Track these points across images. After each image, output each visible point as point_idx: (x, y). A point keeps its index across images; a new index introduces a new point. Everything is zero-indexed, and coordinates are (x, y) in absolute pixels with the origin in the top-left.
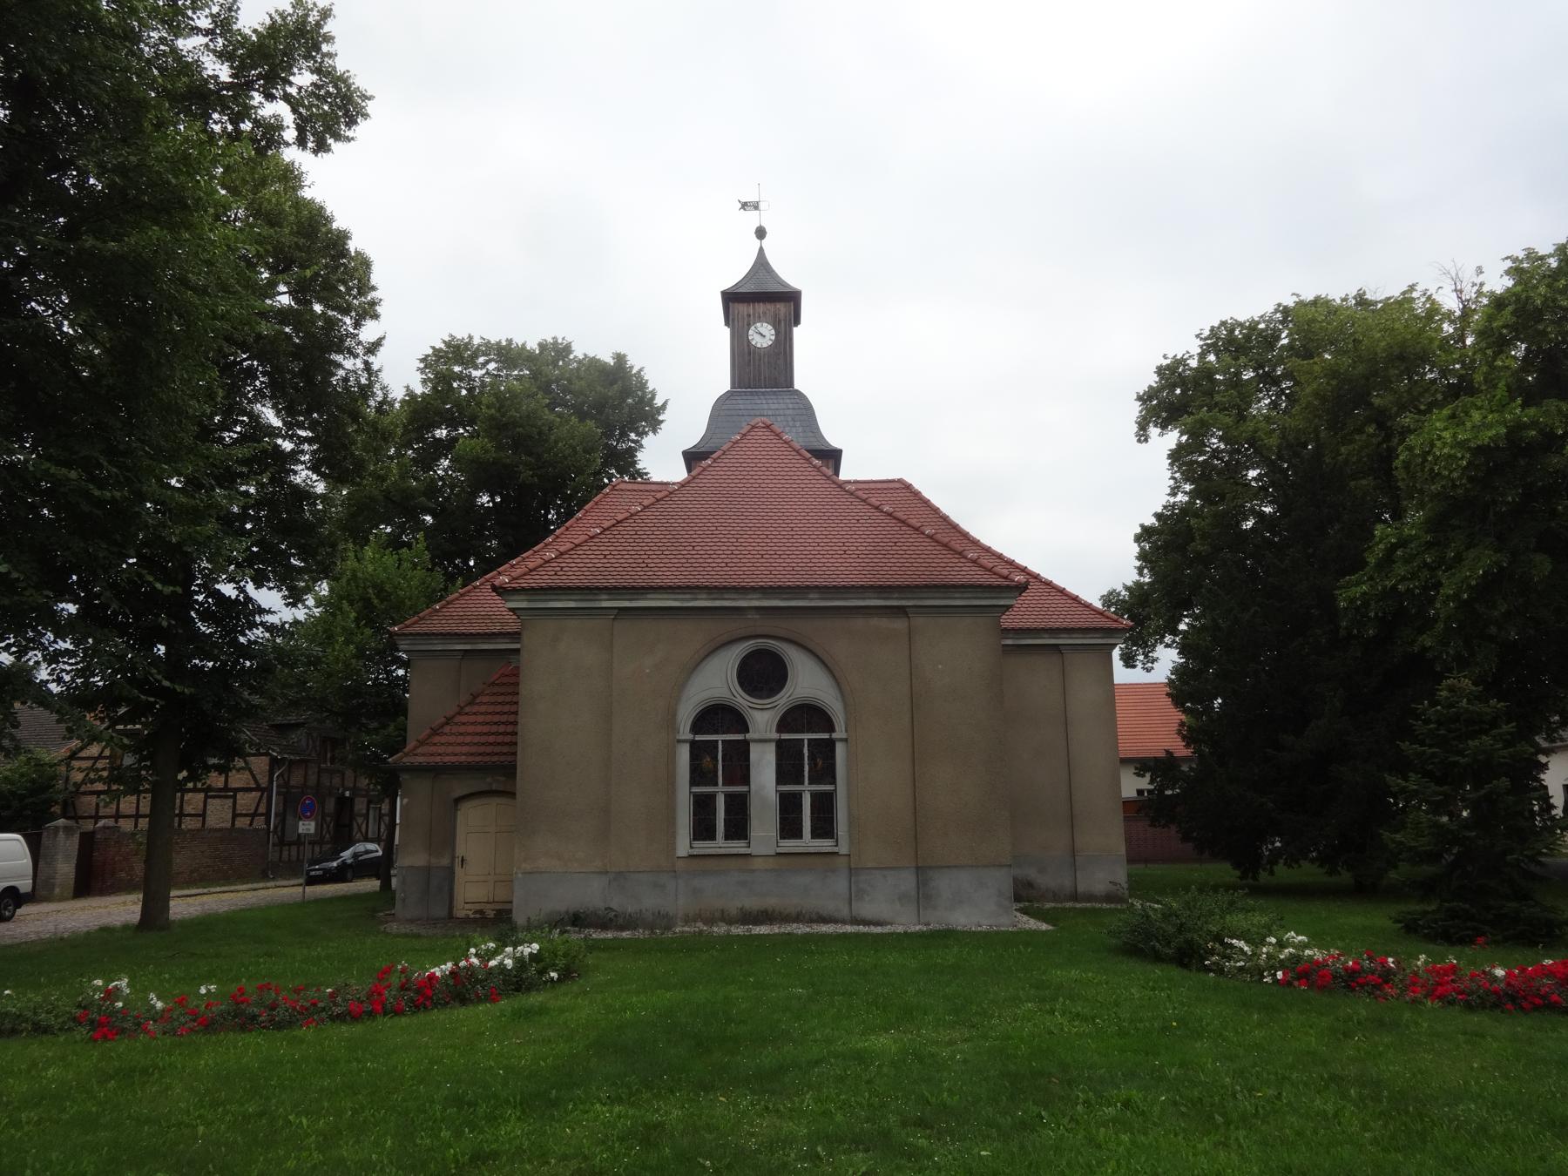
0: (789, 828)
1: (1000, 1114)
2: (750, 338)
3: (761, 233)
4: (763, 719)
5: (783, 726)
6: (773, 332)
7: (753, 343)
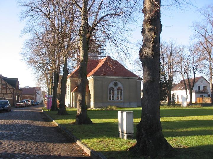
0: (118, 99)
4: (116, 88)
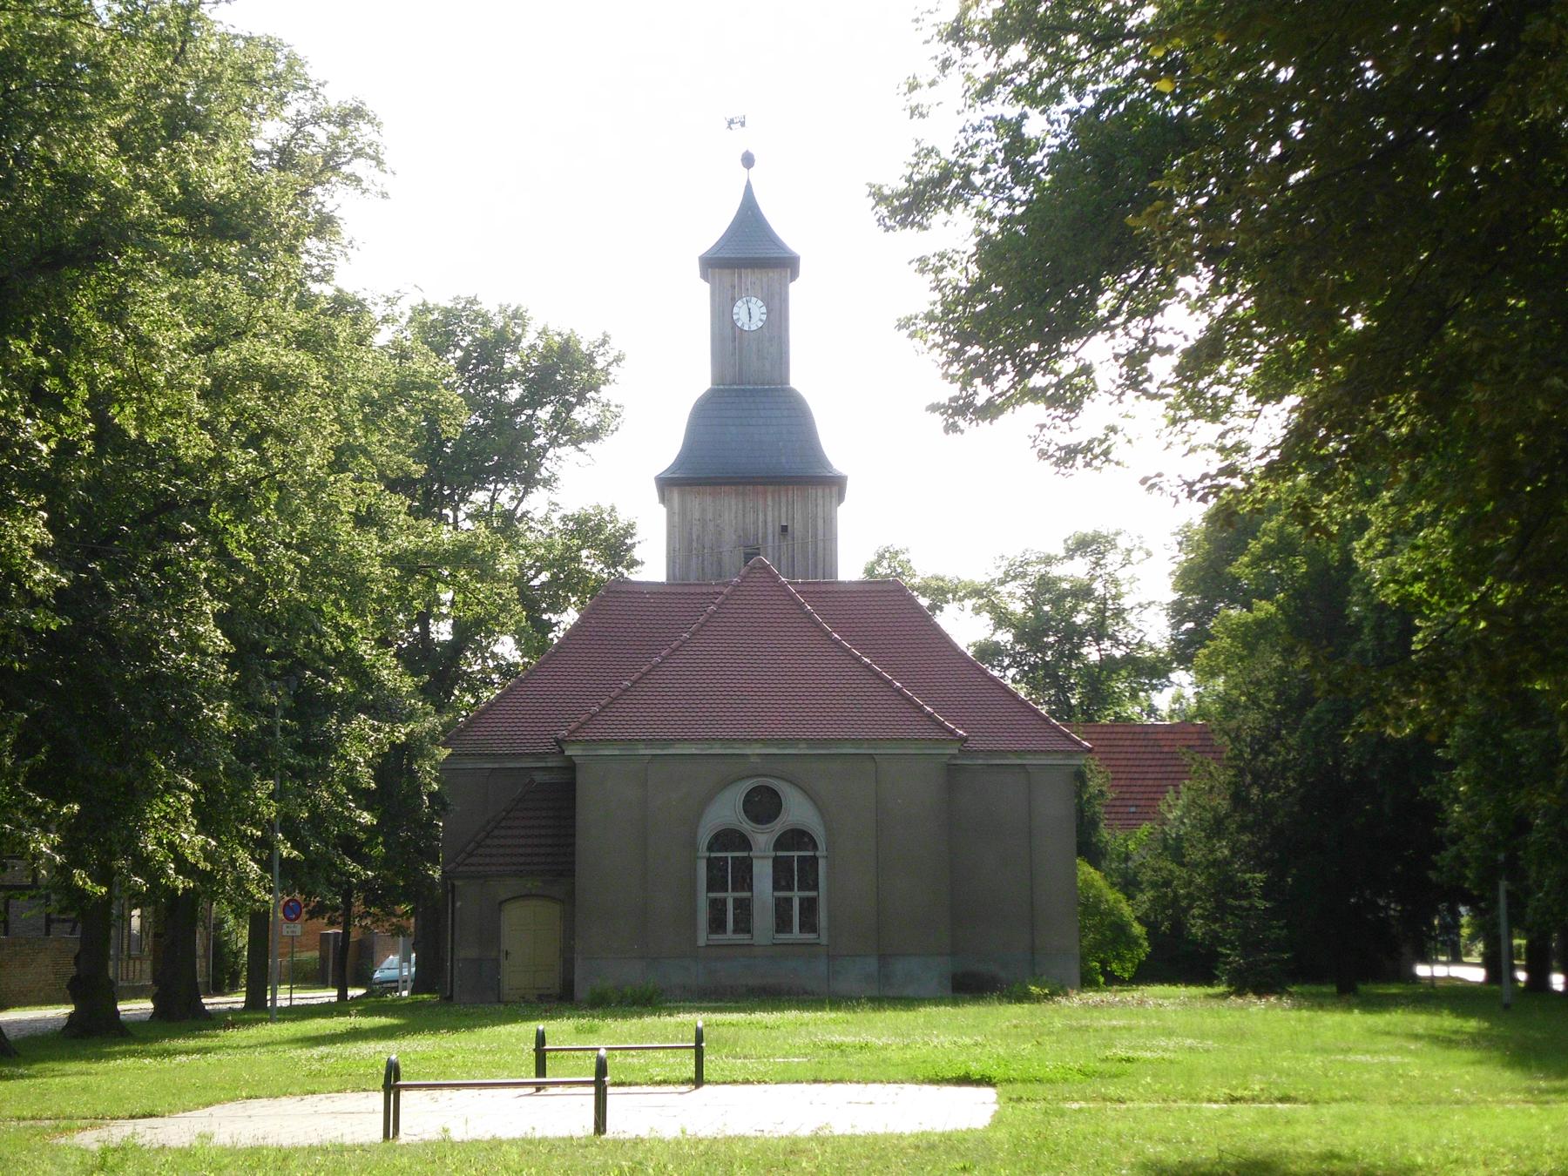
0: (783, 923)
1: (210, 461)
2: (735, 317)
3: (748, 161)
4: (763, 839)
5: (780, 844)
6: (764, 310)
7: (739, 324)
